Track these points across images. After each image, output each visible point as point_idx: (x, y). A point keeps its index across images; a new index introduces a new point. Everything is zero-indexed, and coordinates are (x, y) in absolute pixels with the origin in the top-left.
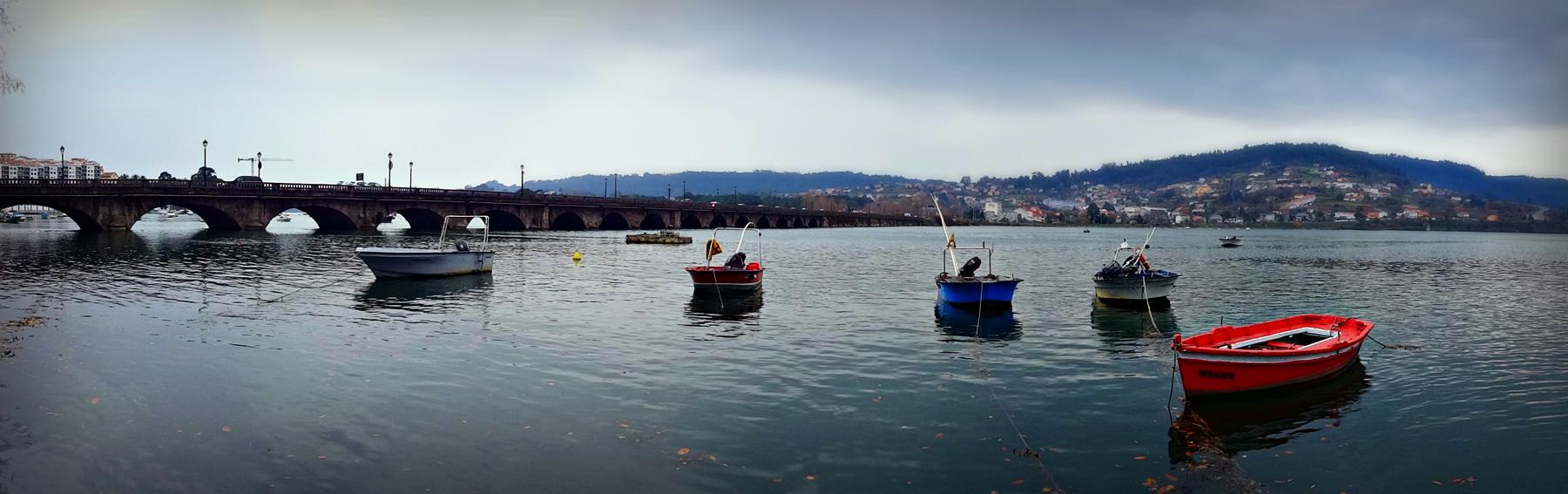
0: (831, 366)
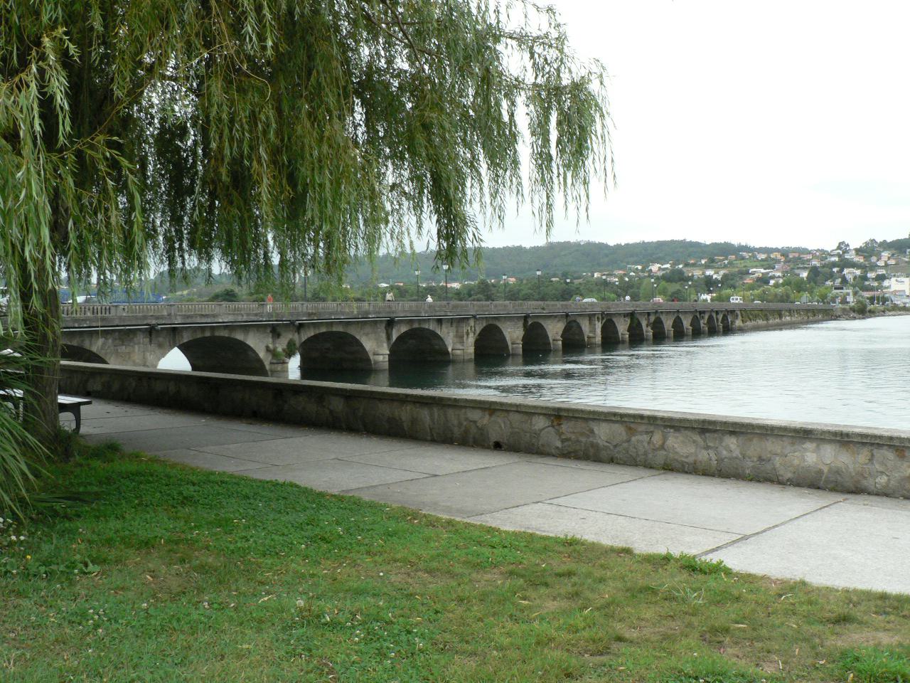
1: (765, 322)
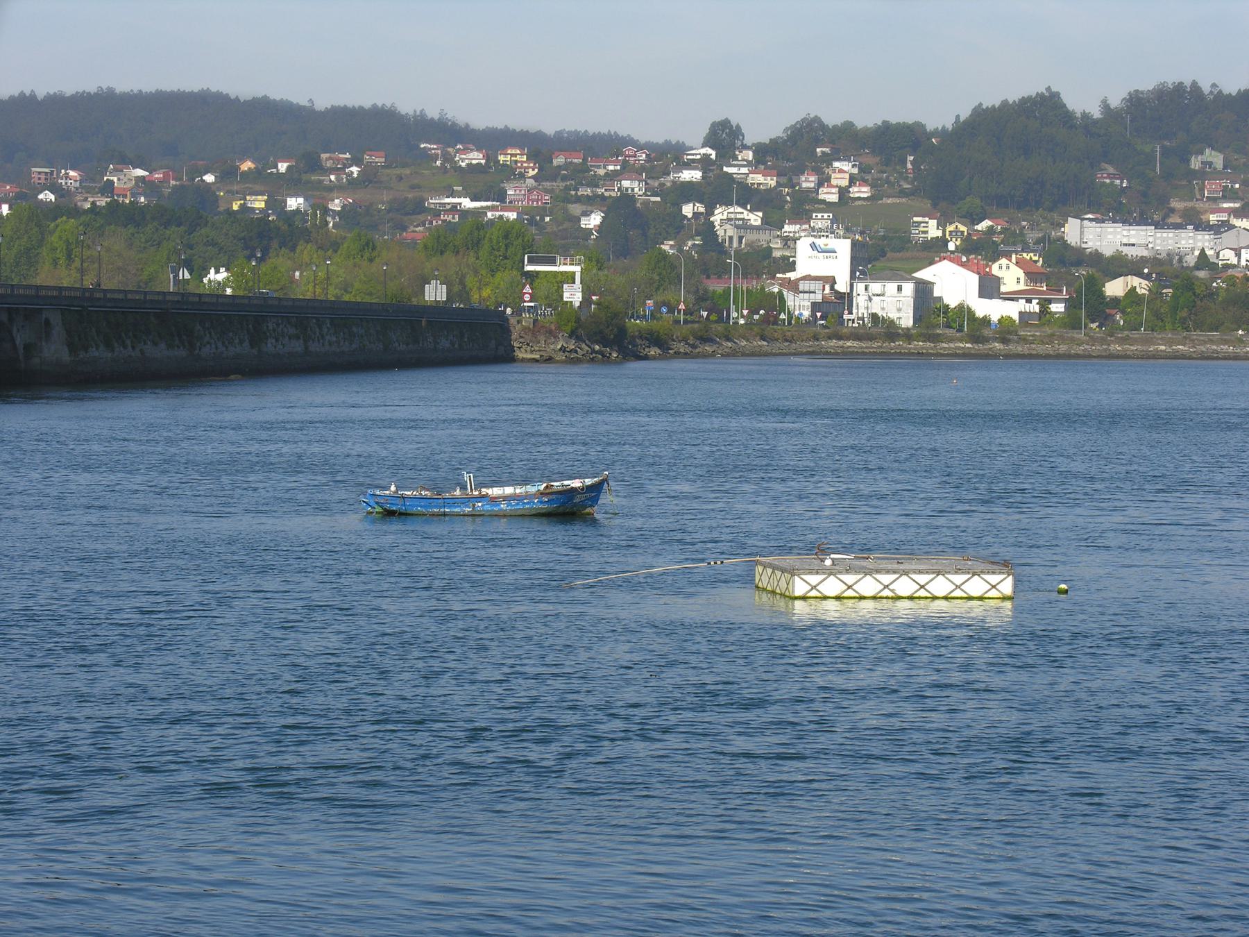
0: (60, 902)
1: (182, 353)
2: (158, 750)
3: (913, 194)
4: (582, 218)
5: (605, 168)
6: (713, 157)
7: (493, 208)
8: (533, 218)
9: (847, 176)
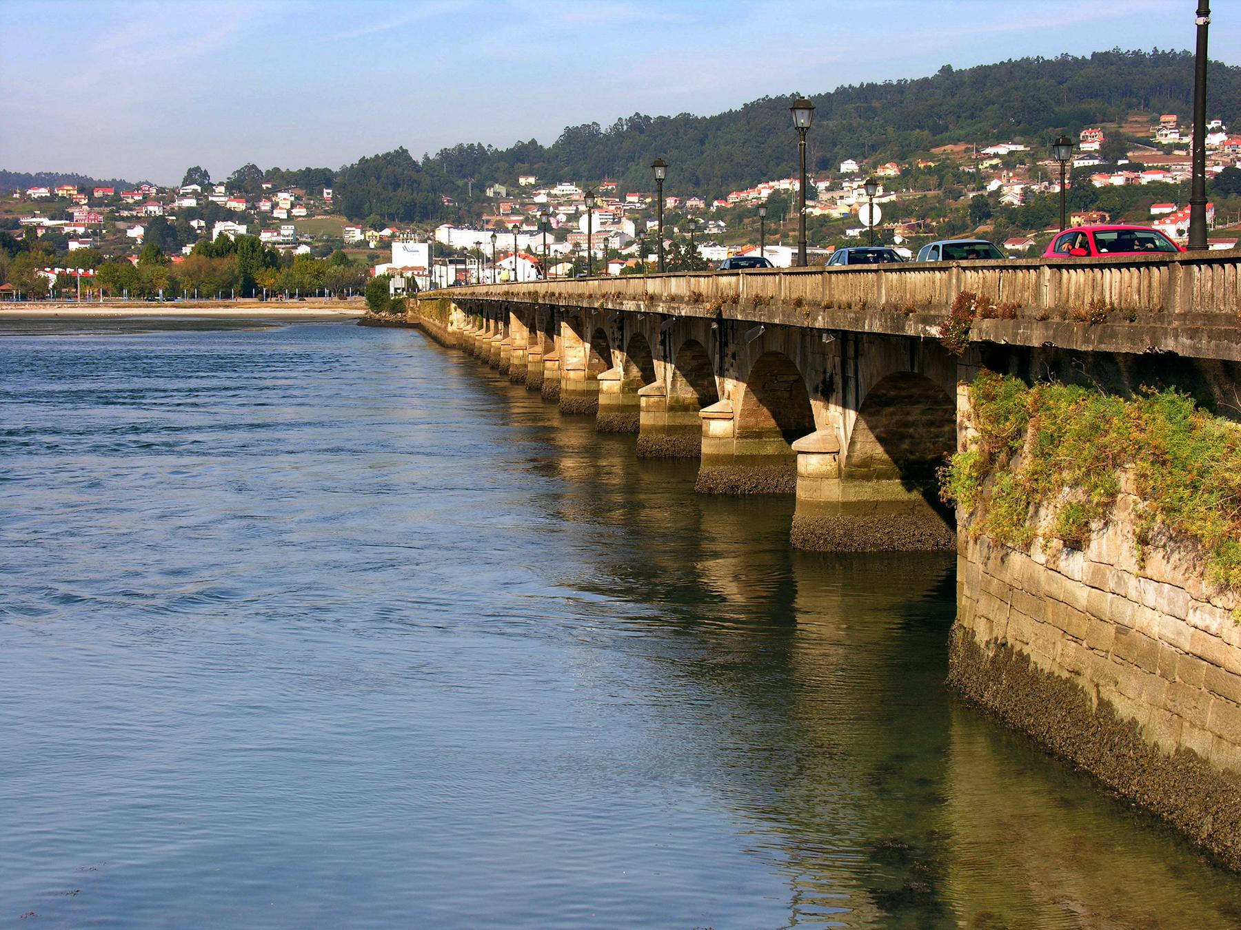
2: (529, 727)
3: (333, 213)
4: (128, 231)
5: (132, 198)
6: (199, 191)
7: (66, 225)
8: (95, 230)
9: (289, 202)
